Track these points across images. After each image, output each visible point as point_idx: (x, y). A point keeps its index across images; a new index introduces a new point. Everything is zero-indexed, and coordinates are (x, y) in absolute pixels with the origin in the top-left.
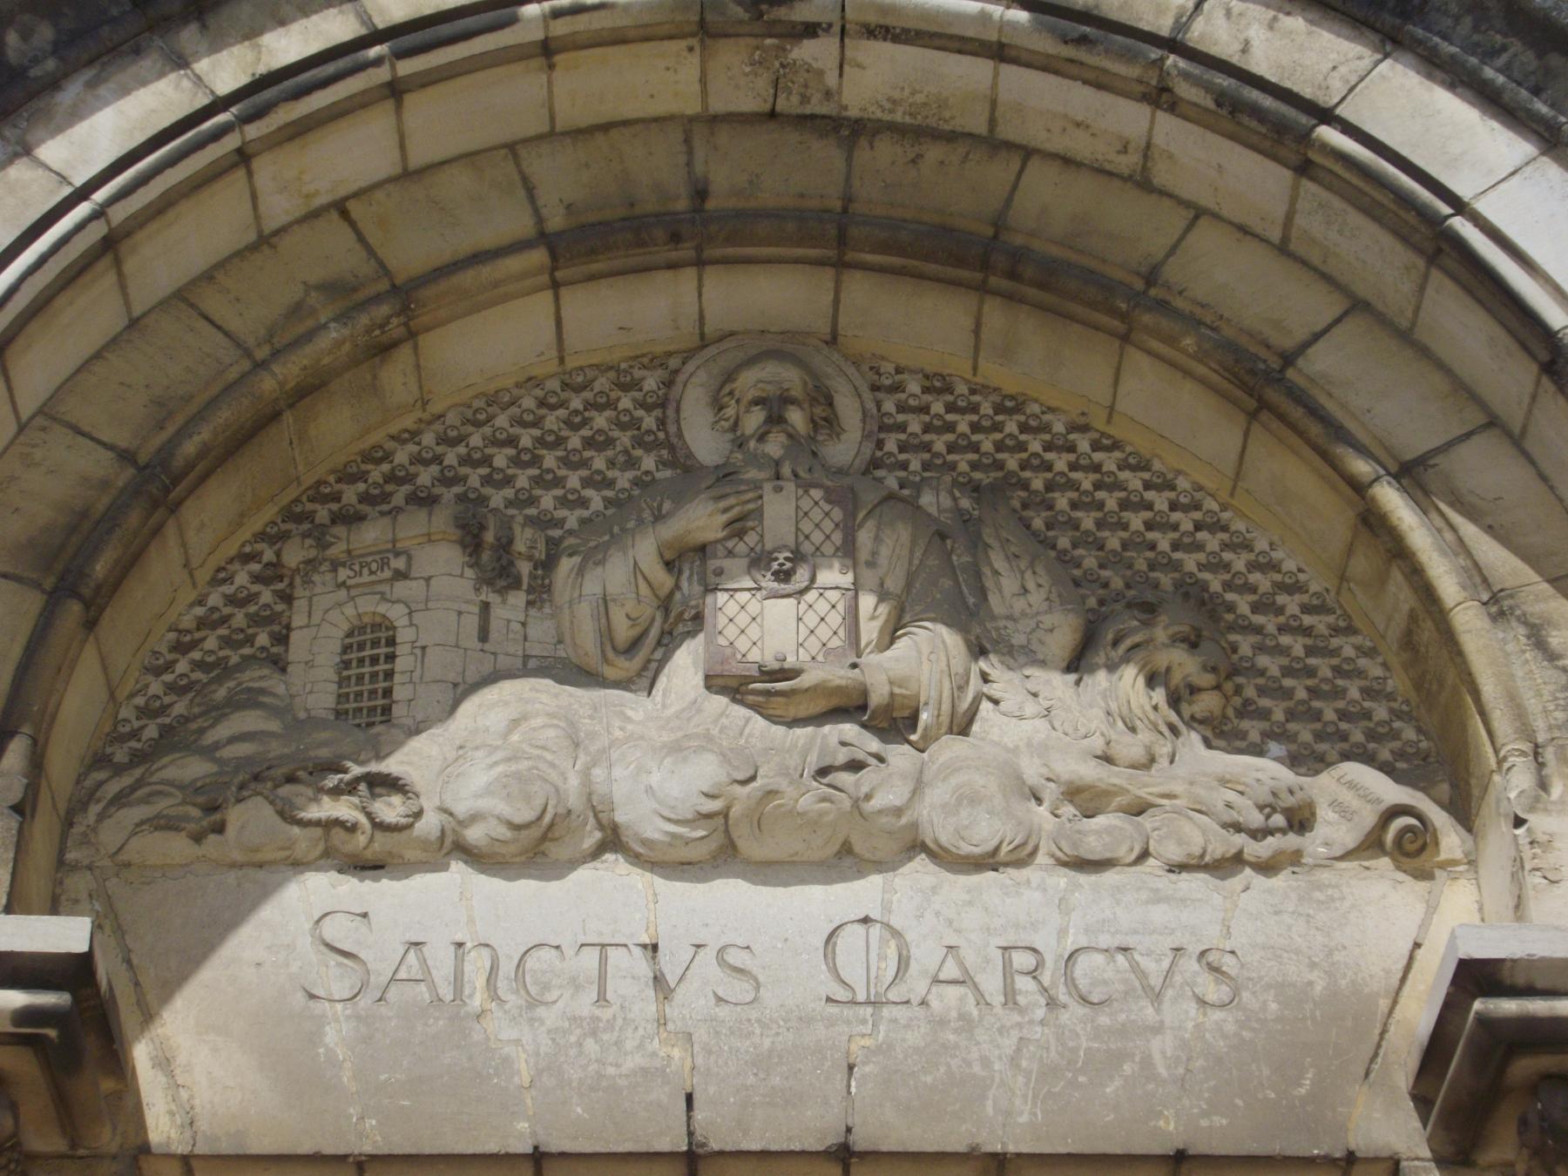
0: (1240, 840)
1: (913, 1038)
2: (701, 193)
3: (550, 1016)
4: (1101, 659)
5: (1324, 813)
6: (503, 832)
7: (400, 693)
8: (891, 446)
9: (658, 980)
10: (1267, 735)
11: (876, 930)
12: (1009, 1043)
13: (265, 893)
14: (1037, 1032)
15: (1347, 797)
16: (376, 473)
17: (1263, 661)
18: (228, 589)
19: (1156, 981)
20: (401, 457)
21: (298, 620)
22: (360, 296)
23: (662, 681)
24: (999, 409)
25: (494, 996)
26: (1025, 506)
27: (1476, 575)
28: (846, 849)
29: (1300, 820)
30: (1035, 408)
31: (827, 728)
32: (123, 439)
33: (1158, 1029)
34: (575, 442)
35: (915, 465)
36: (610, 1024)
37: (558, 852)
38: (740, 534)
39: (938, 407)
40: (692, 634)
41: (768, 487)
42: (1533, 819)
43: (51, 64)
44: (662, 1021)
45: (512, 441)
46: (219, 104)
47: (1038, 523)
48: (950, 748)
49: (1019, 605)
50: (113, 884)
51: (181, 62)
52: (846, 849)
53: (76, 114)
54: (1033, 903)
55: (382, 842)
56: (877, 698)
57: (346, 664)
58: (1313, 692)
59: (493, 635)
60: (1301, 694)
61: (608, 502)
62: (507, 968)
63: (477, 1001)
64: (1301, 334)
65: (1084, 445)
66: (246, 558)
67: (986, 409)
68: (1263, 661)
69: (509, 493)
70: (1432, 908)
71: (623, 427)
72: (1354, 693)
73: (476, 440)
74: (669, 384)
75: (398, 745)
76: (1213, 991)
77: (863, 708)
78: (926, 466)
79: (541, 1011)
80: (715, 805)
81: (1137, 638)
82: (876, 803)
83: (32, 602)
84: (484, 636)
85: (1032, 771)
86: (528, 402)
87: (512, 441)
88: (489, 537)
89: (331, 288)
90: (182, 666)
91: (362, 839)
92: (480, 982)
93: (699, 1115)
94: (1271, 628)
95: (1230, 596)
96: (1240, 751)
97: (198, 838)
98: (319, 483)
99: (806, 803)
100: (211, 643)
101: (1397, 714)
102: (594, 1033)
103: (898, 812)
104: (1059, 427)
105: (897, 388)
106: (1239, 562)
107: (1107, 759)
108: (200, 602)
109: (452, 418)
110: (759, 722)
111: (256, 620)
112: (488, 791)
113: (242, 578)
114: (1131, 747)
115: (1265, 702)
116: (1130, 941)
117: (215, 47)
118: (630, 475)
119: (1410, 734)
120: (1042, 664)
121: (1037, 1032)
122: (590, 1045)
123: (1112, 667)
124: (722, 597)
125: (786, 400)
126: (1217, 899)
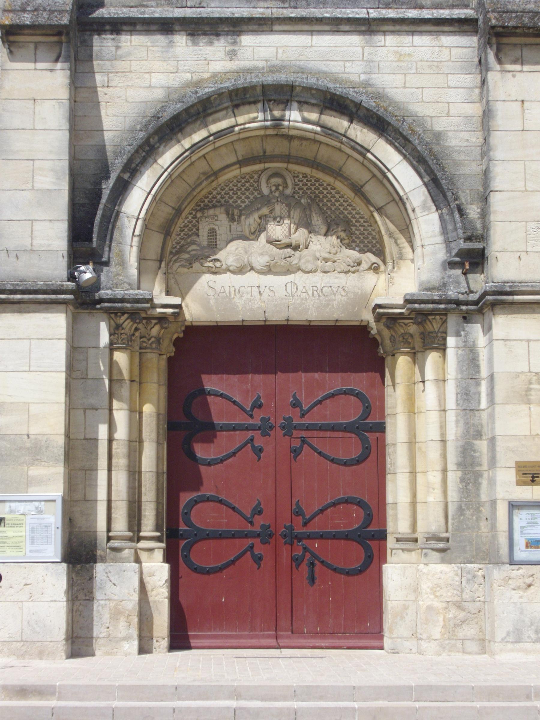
0: (349, 268)
1: (298, 302)
2: (265, 152)
3: (244, 298)
4: (330, 234)
5: (363, 262)
6: (235, 268)
7: (218, 243)
8: (297, 189)
9: (260, 292)
10: (356, 246)
11: (293, 284)
12: (312, 303)
13: (199, 277)
14: (317, 301)
15: (367, 260)
16: (210, 196)
17: (356, 232)
18: (188, 220)
19: (335, 292)
20: (214, 193)
21: (200, 228)
22: (209, 174)
23: (259, 239)
24: (315, 181)
25: (235, 295)
26: (319, 201)
27: (387, 229)
28: (288, 270)
29: (359, 264)
30: (321, 181)
31: (285, 250)
32: (173, 205)
33: (335, 300)
34: (243, 189)
35: (301, 193)
36: (253, 300)
37: (243, 270)
38: (272, 213)
39: (305, 181)
40: (264, 231)
41: (276, 204)
42: (391, 274)
43: (158, 145)
44: (260, 299)
45: (233, 189)
46: (186, 151)
47: (321, 205)
48: (305, 252)
49: (317, 223)
50: (176, 276)
51: (179, 142)
52: (288, 270)
53: (163, 153)
54: (317, 279)
55: (217, 270)
56: (294, 244)
57: (209, 236)
58: (364, 238)
59: (232, 231)
60: (362, 238)
61: (249, 202)
62: (237, 290)
63: (233, 296)
64: (364, 182)
65: (329, 189)
66: (191, 214)
67: (313, 181)
68: (356, 232)
69: (233, 200)
70: (378, 279)
71: (251, 186)
72: (370, 238)
73: (226, 189)
74: (259, 177)
75: (218, 253)
76: (344, 294)
77: (291, 245)
78: (303, 193)
79: (242, 298)
80: (268, 264)
81: (336, 230)
82: (293, 263)
83: (162, 236)
84: (230, 232)
85: (318, 255)
86: (235, 181)
87: (233, 189)
88: (230, 213)
89: (204, 173)
90: (182, 234)
91: (214, 269)
92: (233, 293)
93: (266, 315)
94: (358, 225)
95: (352, 219)
96: (351, 249)
97: (188, 269)
98: (201, 199)
99: (282, 264)
100: (186, 230)
101: (377, 242)
102: (250, 301)
103: (296, 264)
104: (325, 185)
105: (298, 177)
106: (354, 212)
107: (330, 253)
108: (184, 222)
109: (222, 185)
110: (275, 248)
111: (193, 226)
112: (233, 261)
113: (190, 218)
114: (333, 251)
115: (356, 240)
116: (332, 285)
117: (184, 138)
118: (253, 196)
119: (378, 246)
120: (320, 234)
121: (317, 301)
122: (250, 303)
123: (331, 235)
124: (269, 225)
125: (279, 185)
126: (345, 278)
